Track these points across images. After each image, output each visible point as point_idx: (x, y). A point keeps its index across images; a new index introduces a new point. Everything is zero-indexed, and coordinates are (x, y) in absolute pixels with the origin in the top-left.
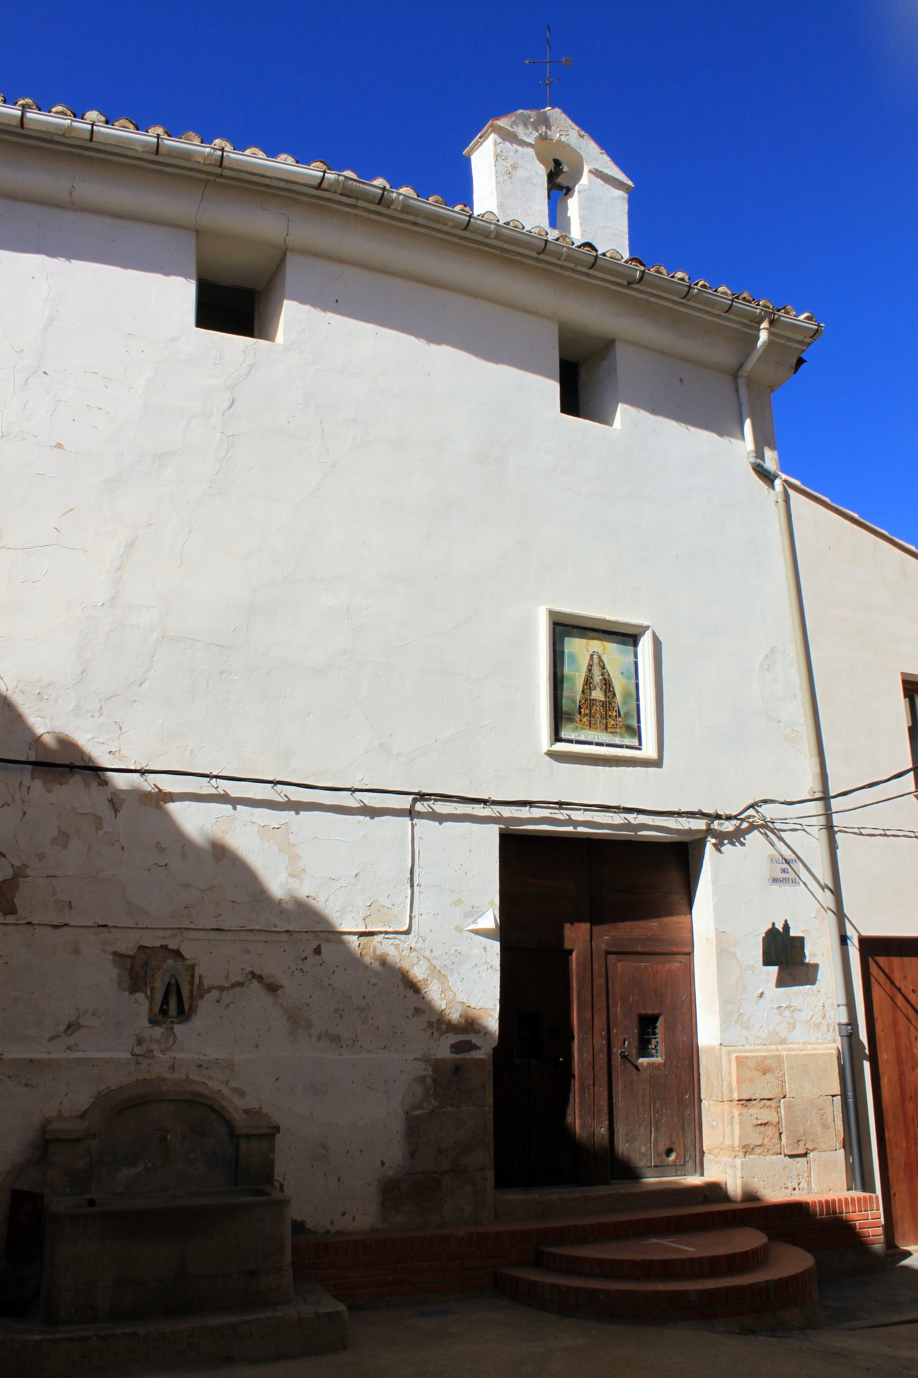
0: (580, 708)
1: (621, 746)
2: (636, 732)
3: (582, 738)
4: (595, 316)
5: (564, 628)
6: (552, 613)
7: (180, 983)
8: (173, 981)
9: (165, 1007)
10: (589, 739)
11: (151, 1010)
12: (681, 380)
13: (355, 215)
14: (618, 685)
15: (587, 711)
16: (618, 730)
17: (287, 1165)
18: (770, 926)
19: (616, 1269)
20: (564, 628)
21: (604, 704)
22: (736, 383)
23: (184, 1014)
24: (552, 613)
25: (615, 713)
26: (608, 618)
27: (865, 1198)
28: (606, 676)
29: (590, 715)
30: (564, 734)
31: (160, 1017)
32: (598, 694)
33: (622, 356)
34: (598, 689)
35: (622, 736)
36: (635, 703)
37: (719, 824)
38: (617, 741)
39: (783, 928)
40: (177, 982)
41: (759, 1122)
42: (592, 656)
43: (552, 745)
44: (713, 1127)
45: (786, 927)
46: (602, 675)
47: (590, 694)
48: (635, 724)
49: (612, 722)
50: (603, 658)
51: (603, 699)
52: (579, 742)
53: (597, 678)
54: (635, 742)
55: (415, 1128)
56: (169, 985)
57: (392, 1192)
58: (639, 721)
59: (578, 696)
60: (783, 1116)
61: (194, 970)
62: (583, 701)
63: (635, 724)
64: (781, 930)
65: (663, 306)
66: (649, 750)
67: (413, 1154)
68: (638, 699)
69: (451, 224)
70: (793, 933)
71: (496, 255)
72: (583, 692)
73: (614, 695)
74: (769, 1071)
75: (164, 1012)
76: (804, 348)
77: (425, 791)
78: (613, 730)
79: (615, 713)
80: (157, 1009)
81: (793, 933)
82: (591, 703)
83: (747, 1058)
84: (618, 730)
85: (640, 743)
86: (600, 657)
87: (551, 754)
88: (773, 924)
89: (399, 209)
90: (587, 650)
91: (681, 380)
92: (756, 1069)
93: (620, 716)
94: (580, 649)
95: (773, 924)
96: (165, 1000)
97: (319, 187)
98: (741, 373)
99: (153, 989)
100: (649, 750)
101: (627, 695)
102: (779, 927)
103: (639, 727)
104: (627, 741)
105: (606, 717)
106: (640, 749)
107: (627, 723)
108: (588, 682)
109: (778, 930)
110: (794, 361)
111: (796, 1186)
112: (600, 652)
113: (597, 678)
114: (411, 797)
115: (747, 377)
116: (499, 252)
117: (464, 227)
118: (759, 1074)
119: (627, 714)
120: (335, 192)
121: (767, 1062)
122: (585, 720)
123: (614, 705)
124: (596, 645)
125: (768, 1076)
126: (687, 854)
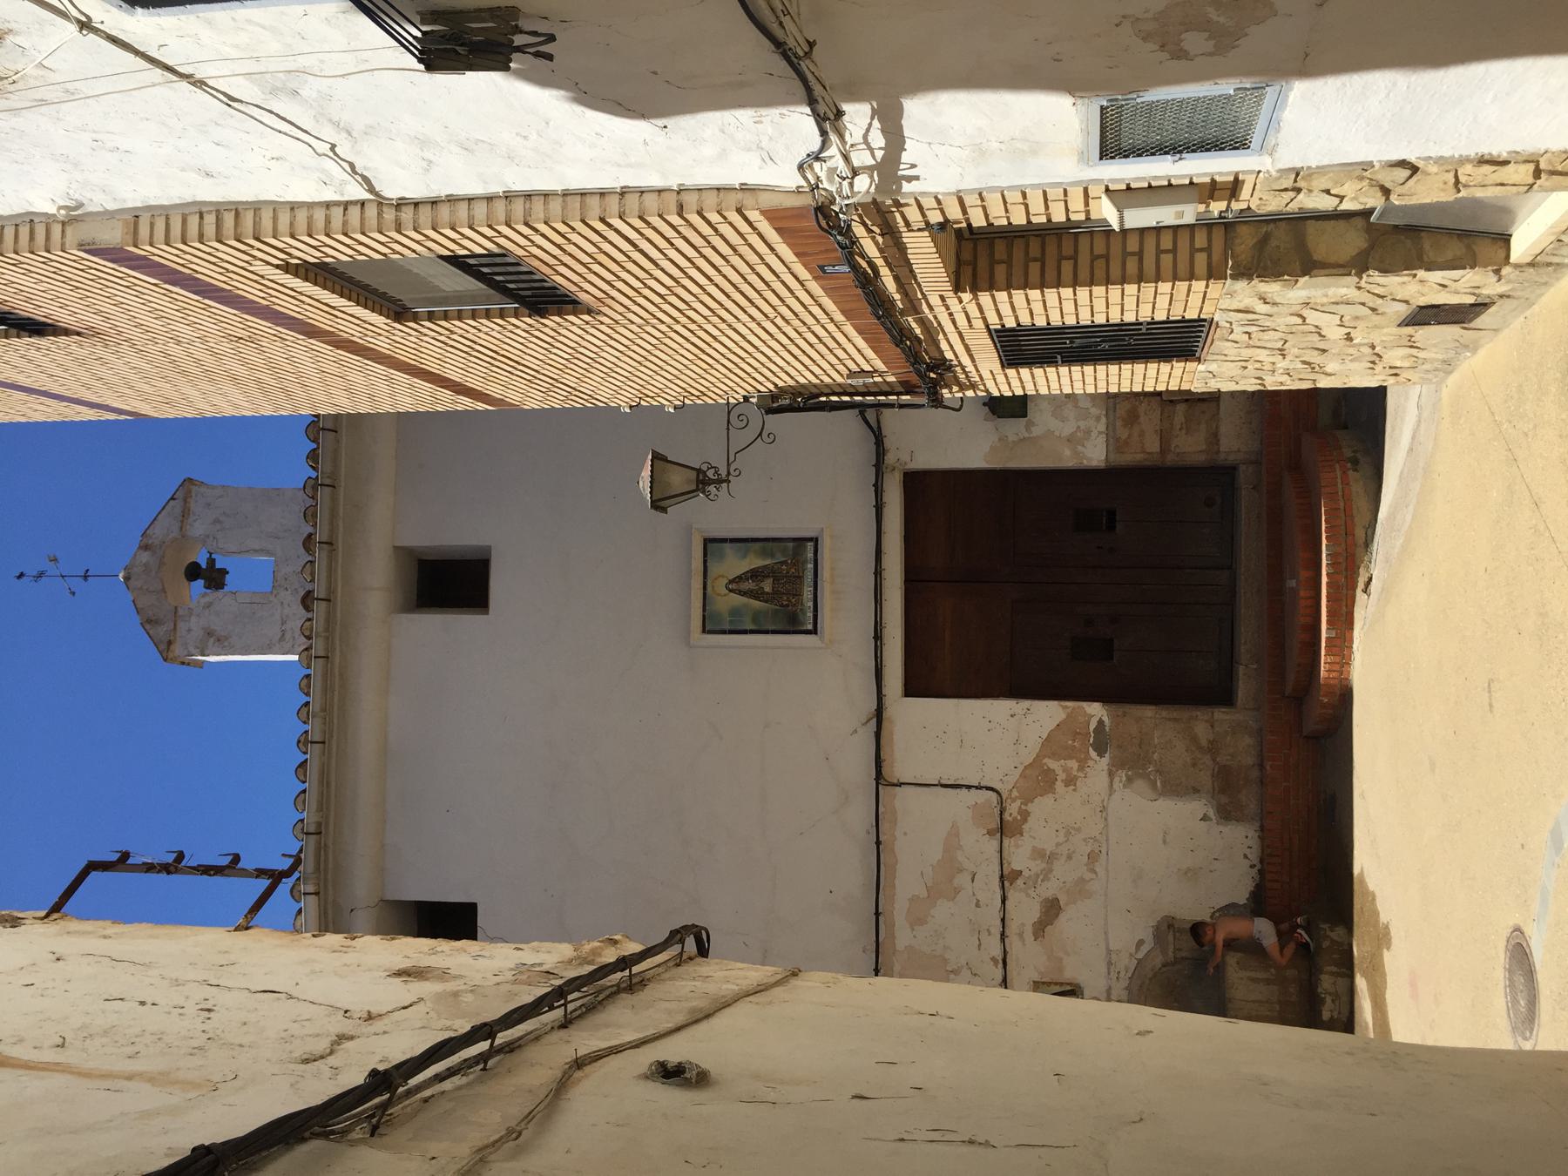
3: (811, 604)
4: (375, 578)
5: (815, 540)
14: (755, 562)
17: (1194, 908)
20: (815, 540)
32: (767, 586)
37: (1180, 215)
53: (748, 585)
55: (1173, 788)
57: (1227, 814)
67: (1196, 791)
70: (218, 566)
71: (483, 1058)
77: (163, 875)
85: (810, 539)
86: (731, 582)
94: (810, 545)
103: (794, 540)
108: (755, 595)
113: (748, 585)
116: (483, 1046)
124: (720, 586)
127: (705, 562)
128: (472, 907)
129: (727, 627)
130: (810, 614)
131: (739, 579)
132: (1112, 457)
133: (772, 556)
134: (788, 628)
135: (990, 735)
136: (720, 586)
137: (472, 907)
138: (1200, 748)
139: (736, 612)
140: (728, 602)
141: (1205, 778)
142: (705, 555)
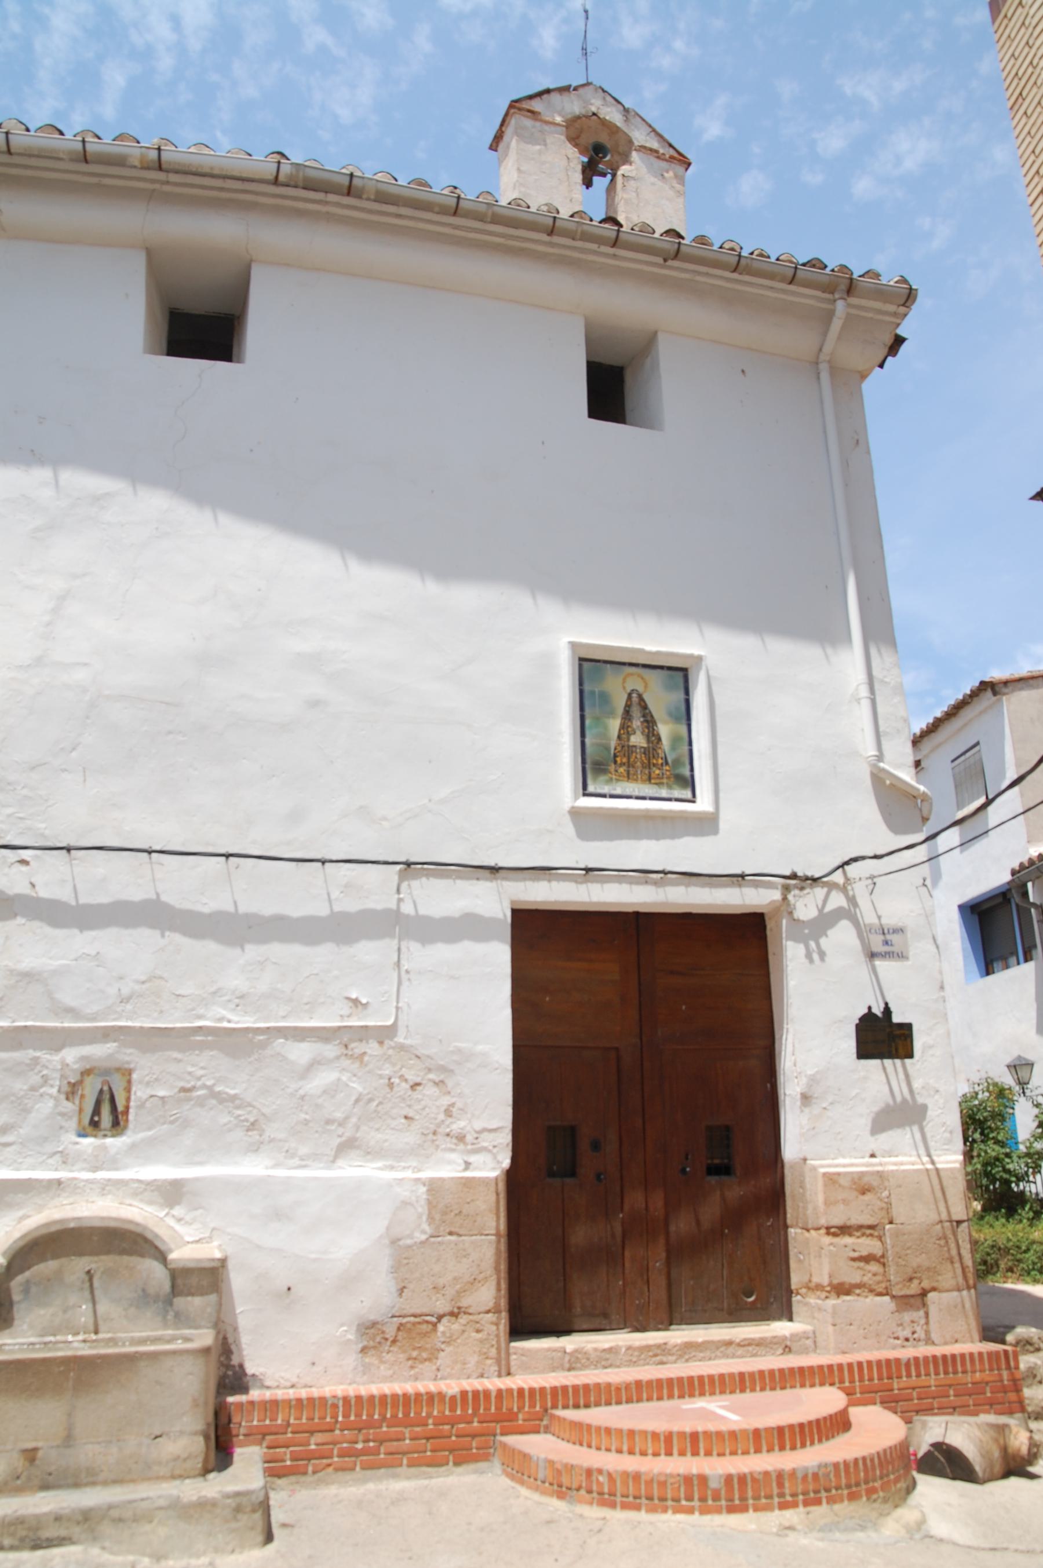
0: (615, 756)
1: (669, 800)
2: (690, 783)
4: (629, 304)
6: (574, 646)
7: (114, 1090)
8: (106, 1088)
9: (96, 1119)
10: (628, 792)
11: (80, 1121)
12: (743, 371)
13: (328, 213)
15: (625, 760)
16: (665, 781)
18: (866, 1011)
19: (631, 1441)
21: (646, 751)
22: (818, 369)
23: (118, 1124)
24: (574, 646)
25: (660, 761)
26: (649, 648)
27: (997, 1353)
28: (649, 718)
29: (629, 765)
30: (591, 789)
31: (89, 1130)
33: (666, 352)
34: (638, 733)
35: (670, 787)
36: (686, 748)
38: (664, 793)
39: (883, 1013)
40: (110, 1089)
41: (856, 1255)
42: (630, 696)
43: (576, 798)
44: (800, 1261)
45: (887, 1011)
46: (644, 716)
47: (628, 740)
48: (687, 773)
49: (657, 772)
50: (645, 697)
51: (645, 745)
52: (612, 796)
54: (687, 794)
55: (403, 1258)
56: (101, 1091)
58: (692, 769)
59: (613, 743)
60: (889, 1247)
61: (130, 1074)
62: (619, 748)
63: (687, 773)
64: (879, 1014)
65: (713, 285)
66: (704, 804)
68: (690, 743)
69: (437, 209)
70: (896, 1019)
72: (619, 737)
73: (659, 739)
74: (869, 1191)
75: (95, 1124)
76: (898, 321)
78: (658, 781)
79: (660, 761)
80: (86, 1120)
81: (896, 1019)
82: (628, 750)
83: (839, 1174)
84: (665, 781)
86: (640, 696)
87: (576, 814)
88: (870, 1008)
89: (372, 197)
90: (624, 688)
91: (743, 371)
92: (851, 1188)
93: (667, 763)
95: (870, 1008)
96: (97, 1111)
97: (276, 182)
98: (822, 357)
99: (82, 1096)
100: (704, 804)
101: (676, 740)
102: (878, 1010)
103: (692, 777)
104: (677, 793)
105: (649, 765)
106: (694, 802)
107: (677, 772)
109: (875, 1015)
110: (889, 340)
111: (909, 1335)
112: (641, 689)
114: (398, 867)
115: (829, 362)
117: (453, 211)
118: (855, 1193)
119: (677, 762)
120: (296, 187)
121: (866, 1179)
122: (621, 770)
123: (660, 751)
124: (634, 683)
125: (868, 1197)
126: (764, 927)
127: (661, 667)
128: (863, 1053)
129: (587, 688)
130: (606, 789)
131: (644, 707)
132: (232, 1407)
133: (673, 748)
134: (589, 760)
135: (468, 1011)
136: (634, 683)
137: (863, 1053)
138: (459, 1293)
139: (604, 699)
140: (617, 688)
141: (418, 1303)
142: (670, 668)
